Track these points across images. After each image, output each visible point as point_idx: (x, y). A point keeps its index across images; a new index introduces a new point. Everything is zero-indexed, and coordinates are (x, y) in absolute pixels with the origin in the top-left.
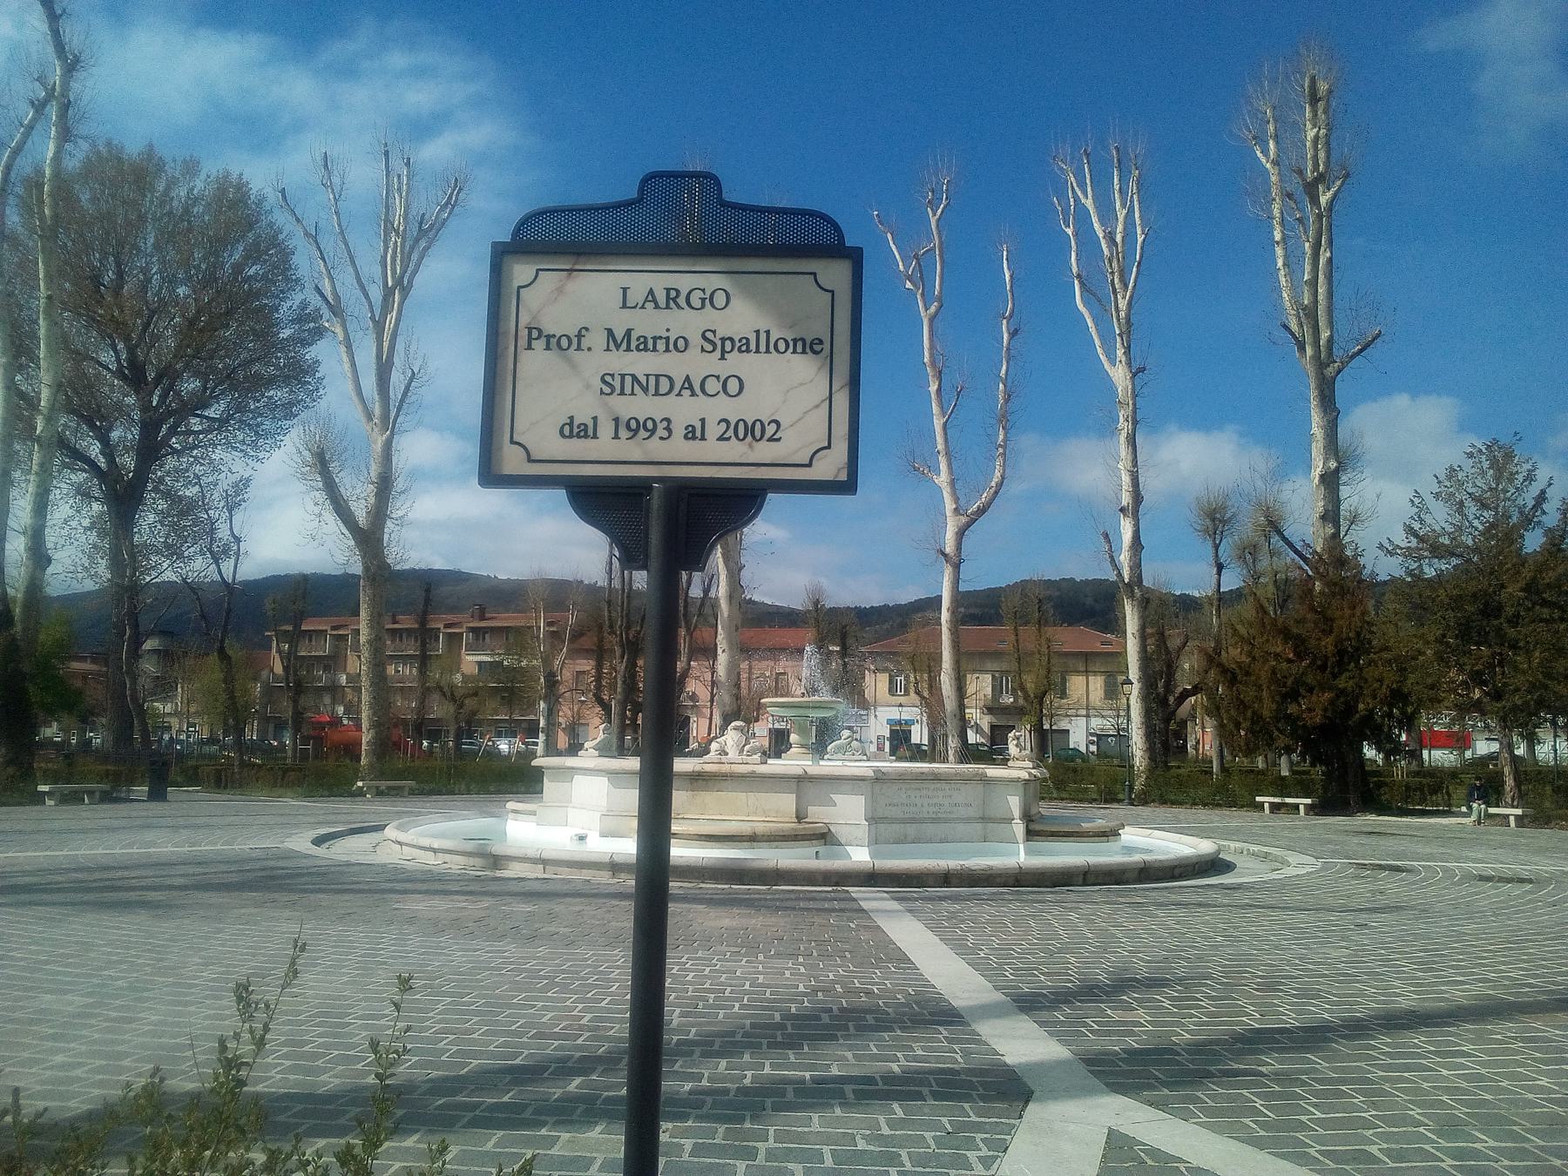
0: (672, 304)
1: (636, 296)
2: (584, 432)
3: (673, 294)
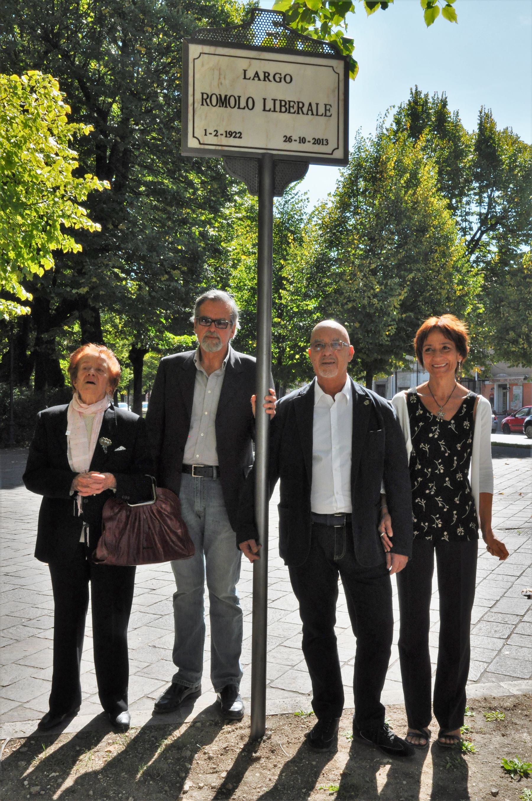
0: (266, 79)
1: (250, 74)
2: (288, 139)
3: (267, 75)
